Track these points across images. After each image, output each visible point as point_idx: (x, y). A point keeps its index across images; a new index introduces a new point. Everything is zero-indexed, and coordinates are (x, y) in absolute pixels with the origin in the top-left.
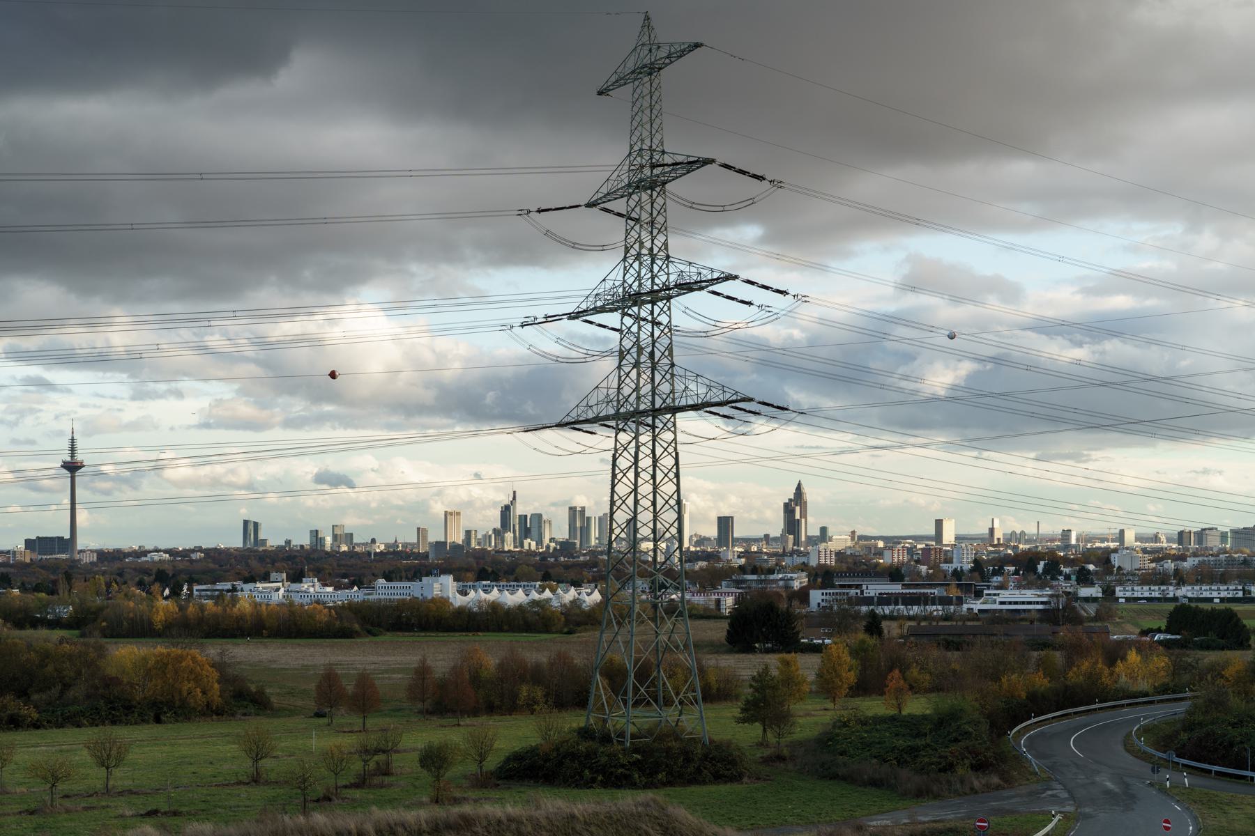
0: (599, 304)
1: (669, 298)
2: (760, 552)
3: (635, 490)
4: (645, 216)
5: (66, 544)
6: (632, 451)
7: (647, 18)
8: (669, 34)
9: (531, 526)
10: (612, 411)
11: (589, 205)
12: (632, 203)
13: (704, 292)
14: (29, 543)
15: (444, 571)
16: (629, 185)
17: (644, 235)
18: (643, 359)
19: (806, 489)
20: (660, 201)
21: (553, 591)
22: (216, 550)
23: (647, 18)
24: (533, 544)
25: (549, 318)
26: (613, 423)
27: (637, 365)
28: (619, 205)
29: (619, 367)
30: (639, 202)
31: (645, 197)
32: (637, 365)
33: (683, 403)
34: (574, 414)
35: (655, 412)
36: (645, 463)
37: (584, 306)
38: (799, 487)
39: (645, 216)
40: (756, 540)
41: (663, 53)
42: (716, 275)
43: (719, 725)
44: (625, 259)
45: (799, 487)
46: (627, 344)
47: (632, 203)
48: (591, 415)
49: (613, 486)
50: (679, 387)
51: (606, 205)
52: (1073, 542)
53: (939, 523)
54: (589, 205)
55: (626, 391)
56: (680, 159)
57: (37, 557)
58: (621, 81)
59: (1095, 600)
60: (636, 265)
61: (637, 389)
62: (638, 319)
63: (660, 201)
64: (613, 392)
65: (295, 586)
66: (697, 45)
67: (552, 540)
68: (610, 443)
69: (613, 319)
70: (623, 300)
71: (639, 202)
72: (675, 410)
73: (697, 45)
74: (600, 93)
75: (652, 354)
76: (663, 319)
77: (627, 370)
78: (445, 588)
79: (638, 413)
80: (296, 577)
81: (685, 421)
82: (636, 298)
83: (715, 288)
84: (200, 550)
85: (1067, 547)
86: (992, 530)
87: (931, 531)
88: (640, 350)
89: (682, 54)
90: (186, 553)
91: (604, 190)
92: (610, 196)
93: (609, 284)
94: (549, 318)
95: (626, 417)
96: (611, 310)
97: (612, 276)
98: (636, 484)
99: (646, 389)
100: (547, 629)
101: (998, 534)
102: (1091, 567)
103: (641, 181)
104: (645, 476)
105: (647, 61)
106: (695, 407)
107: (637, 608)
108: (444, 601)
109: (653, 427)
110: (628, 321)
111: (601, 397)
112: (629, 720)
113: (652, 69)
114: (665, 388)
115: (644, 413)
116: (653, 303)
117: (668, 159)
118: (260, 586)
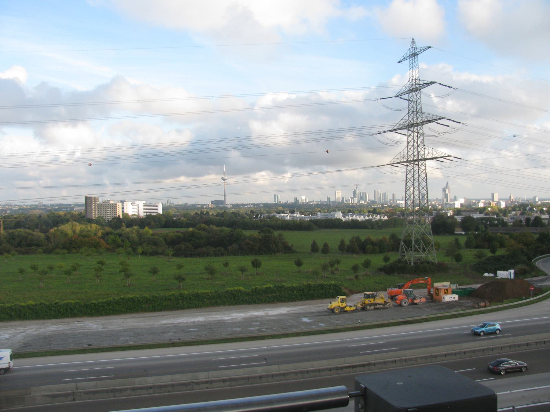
0: (400, 127)
1: (423, 125)
2: (435, 204)
3: (413, 185)
4: (414, 99)
5: (222, 202)
6: (412, 172)
7: (413, 39)
8: (420, 44)
9: (362, 196)
10: (405, 160)
11: (396, 97)
12: (410, 96)
13: (434, 123)
14: (212, 202)
15: (339, 210)
16: (409, 90)
17: (414, 105)
18: (415, 143)
19: (449, 184)
20: (419, 95)
21: (372, 216)
22: (266, 204)
23: (413, 39)
24: (363, 202)
25: (385, 132)
26: (405, 164)
27: (413, 146)
28: (406, 96)
29: (408, 146)
30: (413, 96)
31: (414, 94)
32: (413, 146)
33: (428, 157)
34: (393, 161)
35: (418, 160)
36: (416, 176)
37: (395, 128)
38: (447, 183)
39: (414, 99)
40: (434, 200)
41: (418, 50)
42: (438, 118)
43: (433, 257)
44: (408, 113)
45: (447, 183)
46: (410, 139)
47: (410, 96)
48: (398, 161)
49: (406, 183)
50: (426, 152)
51: (401, 97)
52: (537, 200)
53: (493, 195)
54: (396, 97)
55: (410, 154)
56: (425, 82)
57: (215, 206)
58: (405, 59)
59: (546, 219)
60: (412, 115)
61: (413, 153)
62: (413, 131)
63: (419, 95)
64: (405, 154)
65: (292, 215)
66: (430, 47)
67: (369, 200)
68: (405, 170)
69: (405, 131)
70: (408, 125)
71: (413, 96)
72: (425, 159)
73: (430, 47)
74: (399, 62)
75: (417, 142)
76: (421, 131)
77: (410, 147)
78: (339, 215)
79: (414, 160)
80: (292, 212)
81: (427, 162)
82: (412, 125)
83: (438, 121)
84: (262, 204)
85: (536, 202)
86: (510, 197)
87: (490, 197)
88: (414, 141)
89: (424, 50)
90: (258, 205)
91: (401, 92)
92: (402, 94)
93: (403, 121)
94: (385, 132)
95: (410, 162)
96: (404, 129)
97: (404, 118)
98: (414, 183)
99: (416, 153)
100: (372, 228)
101: (512, 198)
102: (544, 209)
103: (413, 89)
104: (416, 180)
105: (413, 52)
106: (433, 159)
107: (415, 221)
108: (339, 220)
109: (418, 165)
110: (410, 132)
111: (402, 155)
112: (411, 256)
113: (414, 55)
114: (422, 153)
115: (416, 160)
116: (418, 126)
117: (421, 82)
118: (282, 215)
